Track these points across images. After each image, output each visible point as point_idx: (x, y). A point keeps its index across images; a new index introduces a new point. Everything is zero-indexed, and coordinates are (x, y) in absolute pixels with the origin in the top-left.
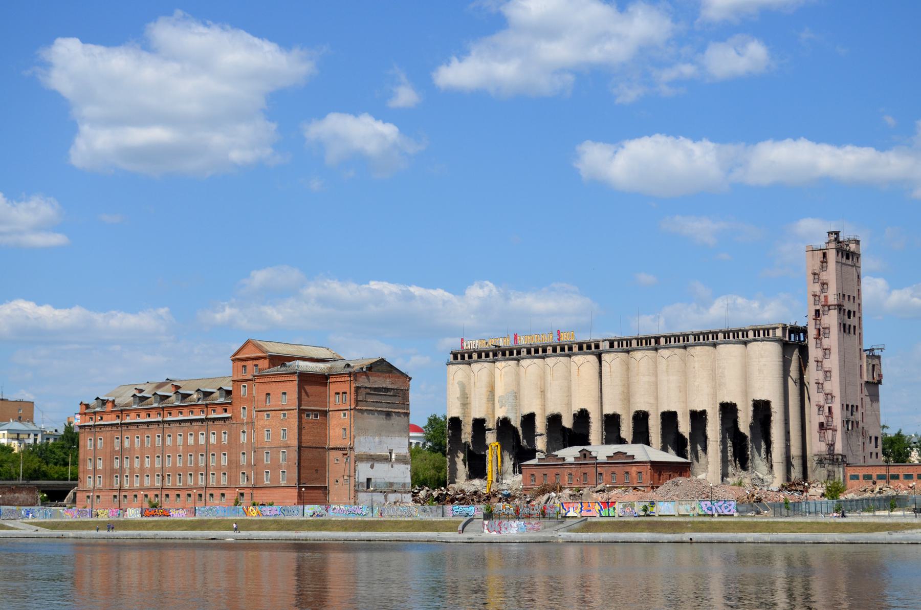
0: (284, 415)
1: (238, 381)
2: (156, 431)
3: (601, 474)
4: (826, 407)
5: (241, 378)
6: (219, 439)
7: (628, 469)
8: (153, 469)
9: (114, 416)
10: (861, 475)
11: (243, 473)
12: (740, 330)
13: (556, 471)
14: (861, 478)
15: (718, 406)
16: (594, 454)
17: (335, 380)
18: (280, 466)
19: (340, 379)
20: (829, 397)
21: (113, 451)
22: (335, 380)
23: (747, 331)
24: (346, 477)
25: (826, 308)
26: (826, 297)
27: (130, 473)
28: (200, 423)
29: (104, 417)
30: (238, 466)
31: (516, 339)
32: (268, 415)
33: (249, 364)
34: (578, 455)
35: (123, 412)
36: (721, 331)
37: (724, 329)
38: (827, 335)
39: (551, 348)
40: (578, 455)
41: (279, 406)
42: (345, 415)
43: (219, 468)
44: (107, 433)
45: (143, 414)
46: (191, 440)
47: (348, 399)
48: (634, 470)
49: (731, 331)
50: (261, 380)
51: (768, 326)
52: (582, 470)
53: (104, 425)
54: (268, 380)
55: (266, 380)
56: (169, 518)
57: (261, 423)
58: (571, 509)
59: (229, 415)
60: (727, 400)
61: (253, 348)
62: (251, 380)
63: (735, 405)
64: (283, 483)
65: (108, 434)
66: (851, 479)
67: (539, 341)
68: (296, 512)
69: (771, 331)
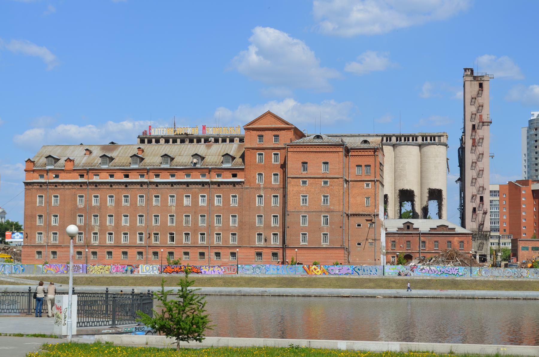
0: (326, 183)
1: (253, 149)
2: (137, 191)
3: (424, 242)
4: (478, 196)
5: (257, 146)
6: (226, 202)
7: (450, 239)
8: (133, 226)
9: (76, 174)
10: (530, 247)
11: (260, 234)
12: (411, 136)
14: (530, 249)
15: (398, 192)
16: (415, 226)
17: (354, 154)
18: (321, 229)
19: (363, 153)
20: (481, 189)
21: (76, 209)
22: (354, 154)
23: (390, 137)
24: (370, 241)
25: (481, 124)
26: (481, 116)
27: (100, 230)
28: (200, 186)
29: (61, 175)
30: (253, 227)
31: (204, 128)
32: (304, 183)
33: (268, 135)
34: (402, 226)
35: (83, 172)
36: (394, 135)
37: (397, 133)
38: (480, 144)
39: (238, 139)
40: (402, 226)
41: (319, 174)
42: (368, 185)
43: (226, 228)
44: (68, 192)
45: (121, 174)
46: (186, 202)
47: (373, 171)
49: (403, 136)
50: (295, 150)
51: (435, 134)
52: (405, 239)
53: (62, 183)
54: (305, 150)
55: (301, 150)
56: (200, 275)
57: (296, 189)
59: (243, 180)
60: (407, 187)
61: (273, 119)
62: (284, 148)
63: (413, 192)
64: (324, 245)
65: (68, 192)
66: (523, 250)
67: (224, 132)
68: (374, 271)
69: (437, 138)
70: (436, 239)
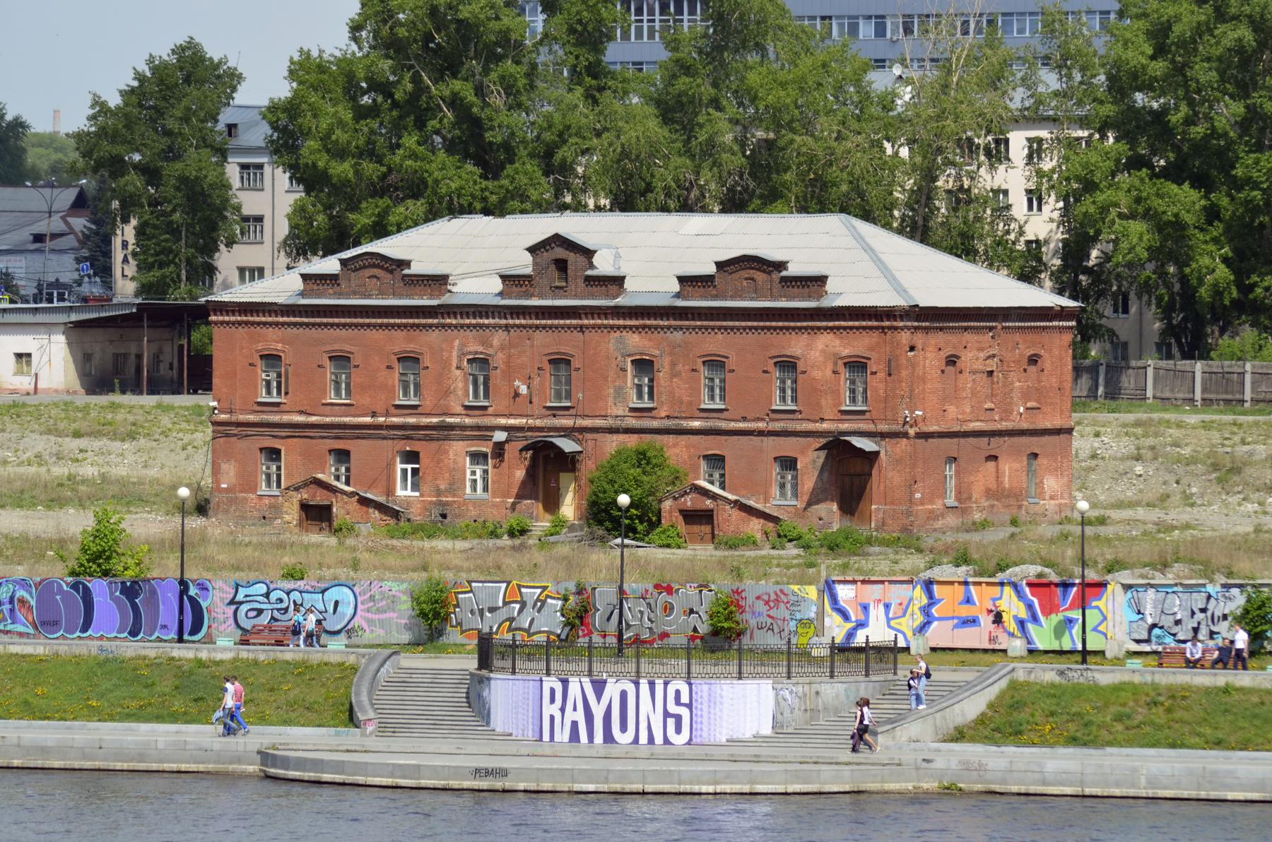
7: (428, 342)
13: (400, 341)
16: (603, 265)
34: (523, 263)
40: (523, 263)
48: (819, 351)
52: (545, 342)
58: (877, 613)
70: (715, 342)
